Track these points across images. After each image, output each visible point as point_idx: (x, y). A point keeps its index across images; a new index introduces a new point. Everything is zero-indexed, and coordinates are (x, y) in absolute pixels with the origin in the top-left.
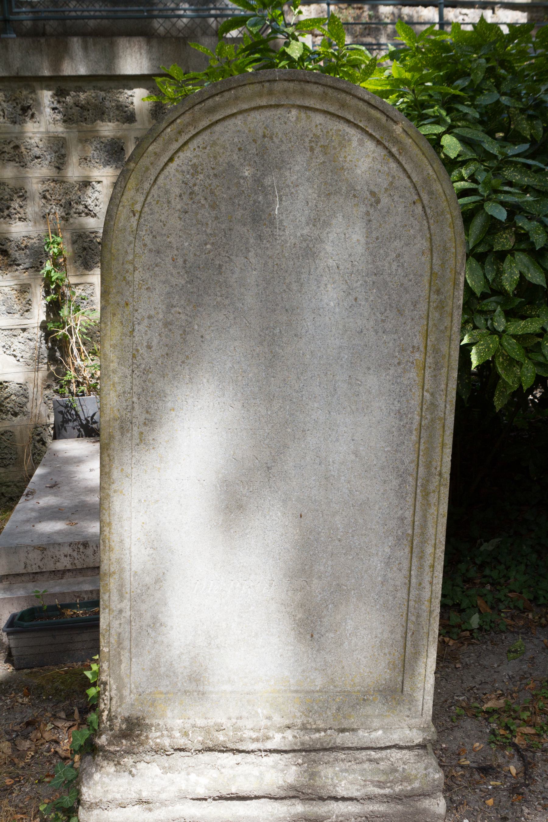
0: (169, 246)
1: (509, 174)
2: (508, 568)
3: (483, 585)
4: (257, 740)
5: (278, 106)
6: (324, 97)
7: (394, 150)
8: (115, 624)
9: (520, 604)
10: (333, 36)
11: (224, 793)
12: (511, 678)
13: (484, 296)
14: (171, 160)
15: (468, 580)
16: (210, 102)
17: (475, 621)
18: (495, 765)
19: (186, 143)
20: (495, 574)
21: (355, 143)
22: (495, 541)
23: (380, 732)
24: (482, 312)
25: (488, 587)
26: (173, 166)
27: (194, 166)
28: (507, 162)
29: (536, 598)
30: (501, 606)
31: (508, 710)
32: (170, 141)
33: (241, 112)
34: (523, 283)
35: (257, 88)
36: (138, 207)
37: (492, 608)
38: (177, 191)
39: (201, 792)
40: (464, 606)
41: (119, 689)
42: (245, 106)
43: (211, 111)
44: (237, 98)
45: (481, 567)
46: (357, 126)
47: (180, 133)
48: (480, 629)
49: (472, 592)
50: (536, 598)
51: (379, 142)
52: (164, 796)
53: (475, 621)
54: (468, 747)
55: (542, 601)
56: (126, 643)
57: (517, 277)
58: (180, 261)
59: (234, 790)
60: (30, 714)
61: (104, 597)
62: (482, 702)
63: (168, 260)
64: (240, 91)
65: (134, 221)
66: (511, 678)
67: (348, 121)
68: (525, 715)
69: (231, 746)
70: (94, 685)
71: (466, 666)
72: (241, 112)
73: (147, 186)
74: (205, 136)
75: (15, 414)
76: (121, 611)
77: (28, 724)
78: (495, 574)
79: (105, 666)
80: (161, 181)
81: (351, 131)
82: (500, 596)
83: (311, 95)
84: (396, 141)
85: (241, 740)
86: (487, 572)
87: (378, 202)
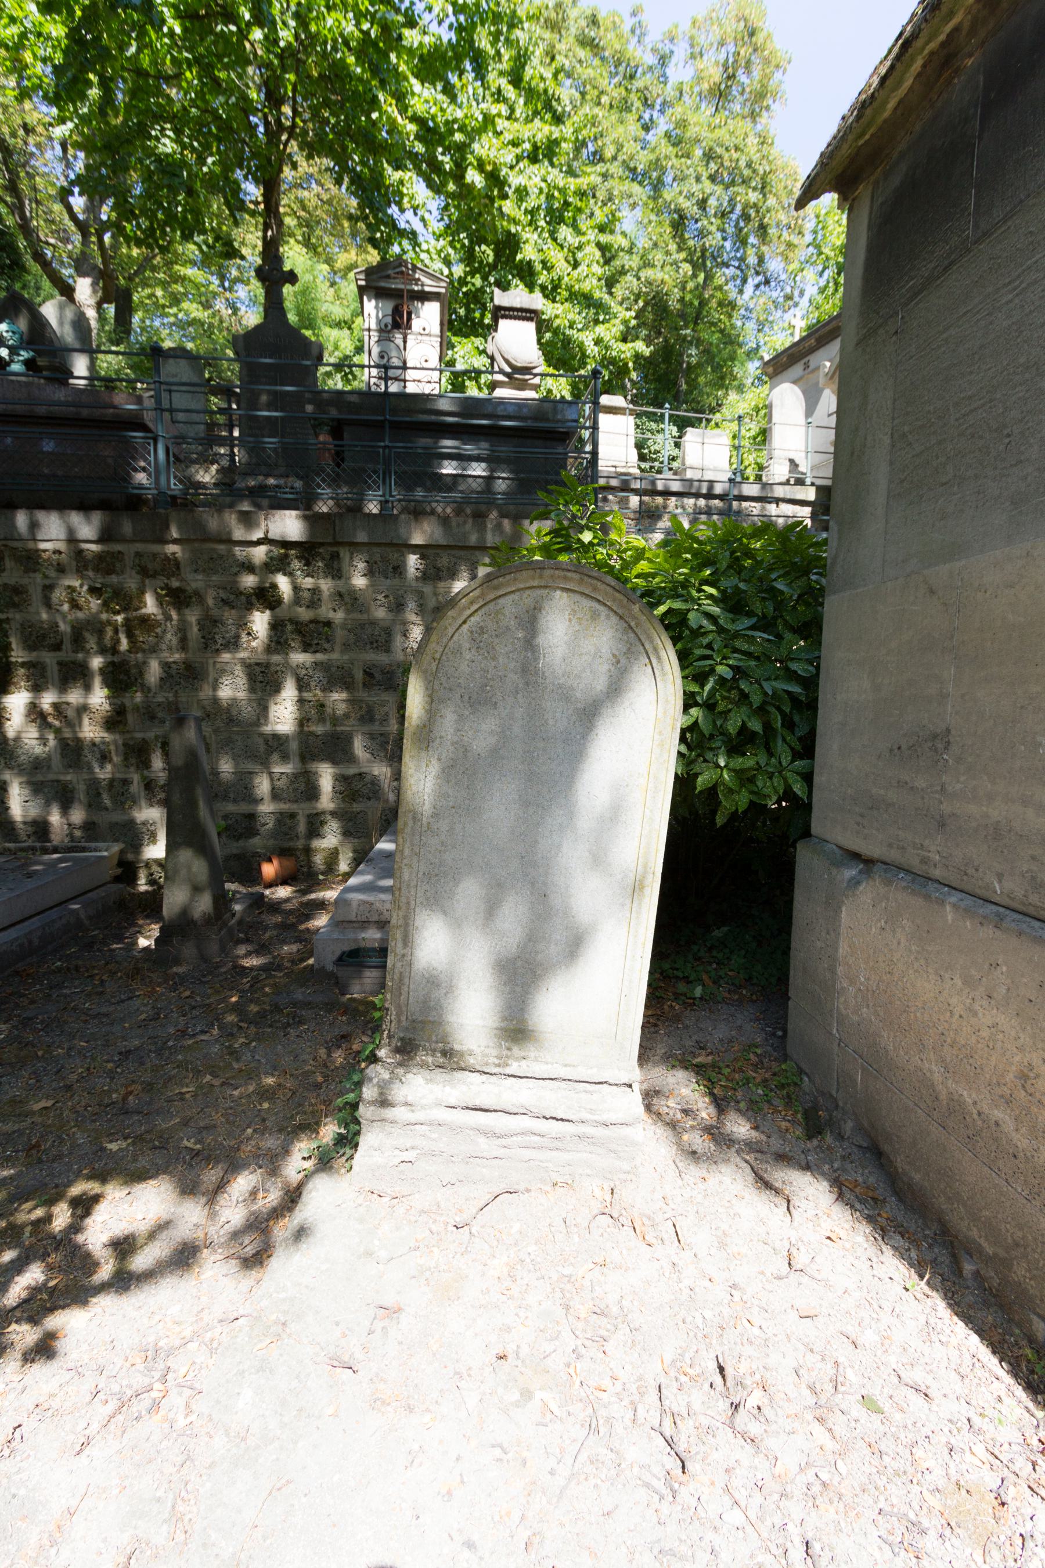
0: (459, 685)
1: (738, 644)
2: (732, 952)
3: (710, 964)
4: (499, 1065)
5: (546, 587)
6: (581, 582)
7: (633, 624)
8: (399, 965)
9: (737, 982)
10: (314, 621)
11: (470, 1105)
12: (721, 1040)
13: (712, 737)
14: (464, 622)
15: (698, 959)
16: (496, 582)
17: (698, 991)
18: (695, 1108)
19: (476, 611)
20: (720, 955)
21: (603, 617)
22: (725, 929)
23: (595, 1070)
24: (711, 749)
25: (714, 966)
26: (465, 627)
27: (481, 628)
28: (736, 635)
29: (750, 978)
30: (722, 982)
31: (714, 1066)
32: (464, 608)
33: (518, 590)
34: (743, 729)
35: (531, 573)
36: (437, 656)
37: (714, 983)
38: (468, 645)
39: (453, 1102)
40: (691, 978)
41: (398, 1015)
42: (522, 586)
43: (496, 588)
44: (515, 579)
45: (710, 949)
46: (605, 605)
47: (472, 603)
48: (701, 999)
49: (701, 968)
50: (750, 978)
51: (621, 618)
52: (424, 1101)
53: (698, 991)
54: (676, 1092)
55: (755, 981)
56: (406, 980)
57: (739, 724)
58: (466, 698)
59: (478, 1103)
60: (345, 1029)
61: (392, 944)
62: (695, 1057)
63: (458, 696)
64: (518, 574)
65: (434, 665)
66: (721, 1040)
67: (599, 601)
68: (726, 1071)
69: (478, 1068)
70: (380, 1009)
71: (687, 1027)
72: (518, 590)
73: (445, 640)
74: (491, 606)
75: (369, 799)
76: (403, 956)
77: (343, 1037)
78: (720, 955)
79: (388, 996)
80: (455, 638)
81: (602, 608)
82: (721, 973)
83: (571, 580)
84: (634, 618)
85: (487, 1064)
86: (714, 953)
87: (618, 662)
